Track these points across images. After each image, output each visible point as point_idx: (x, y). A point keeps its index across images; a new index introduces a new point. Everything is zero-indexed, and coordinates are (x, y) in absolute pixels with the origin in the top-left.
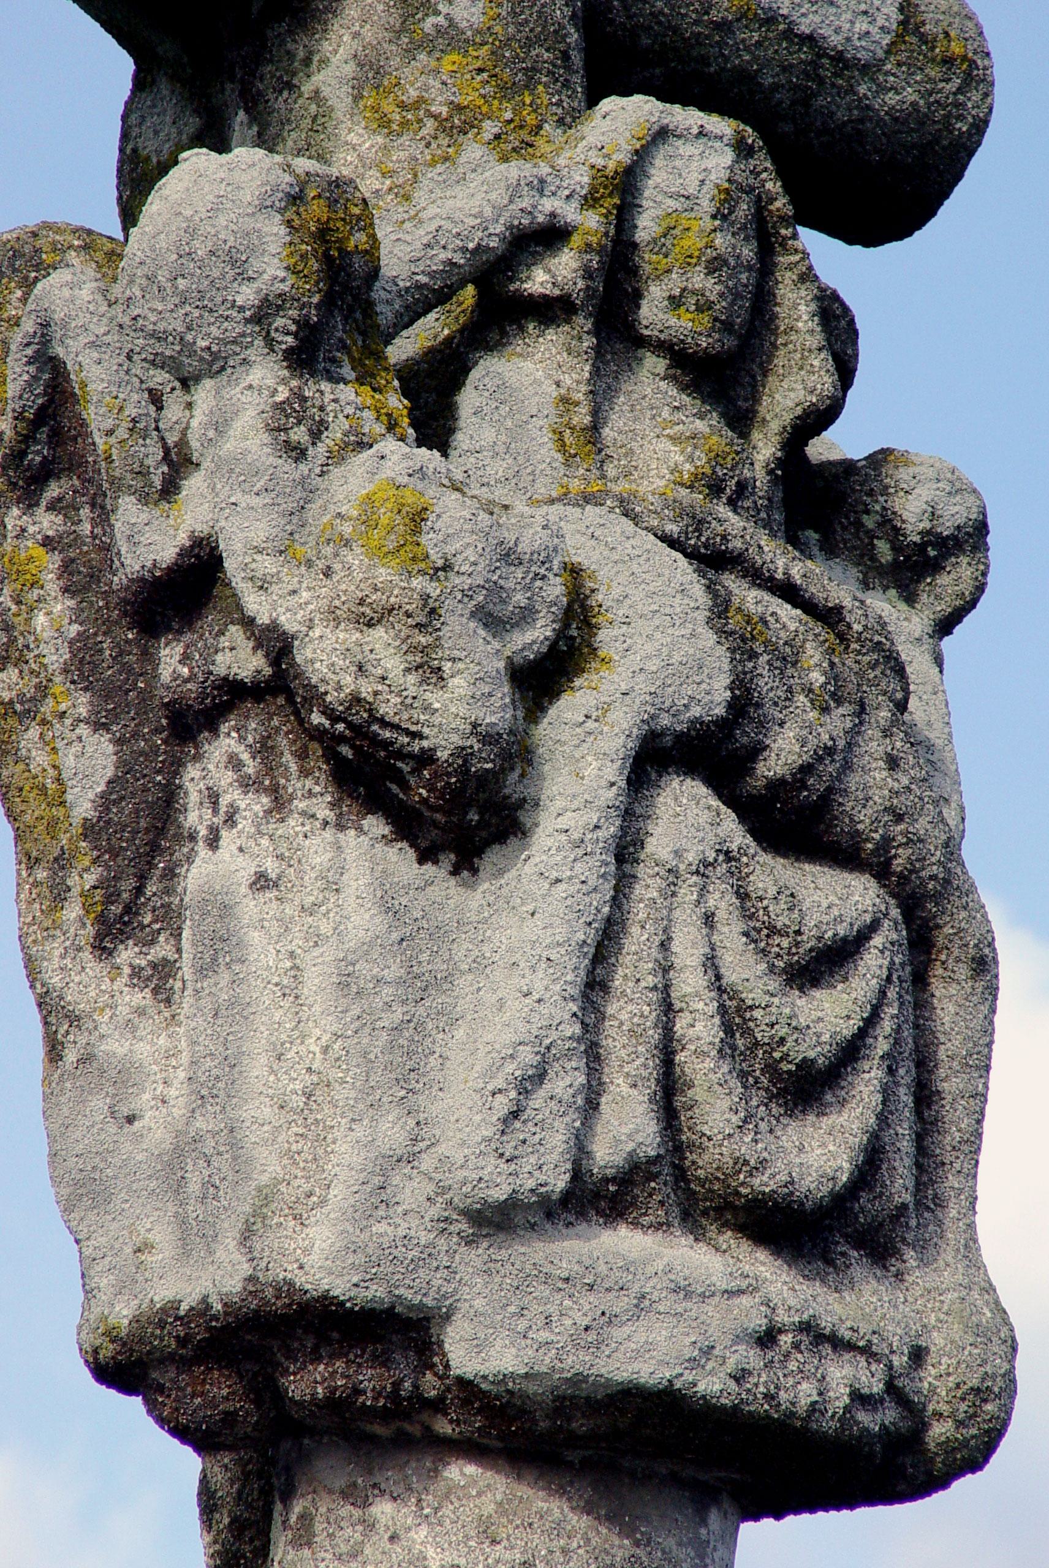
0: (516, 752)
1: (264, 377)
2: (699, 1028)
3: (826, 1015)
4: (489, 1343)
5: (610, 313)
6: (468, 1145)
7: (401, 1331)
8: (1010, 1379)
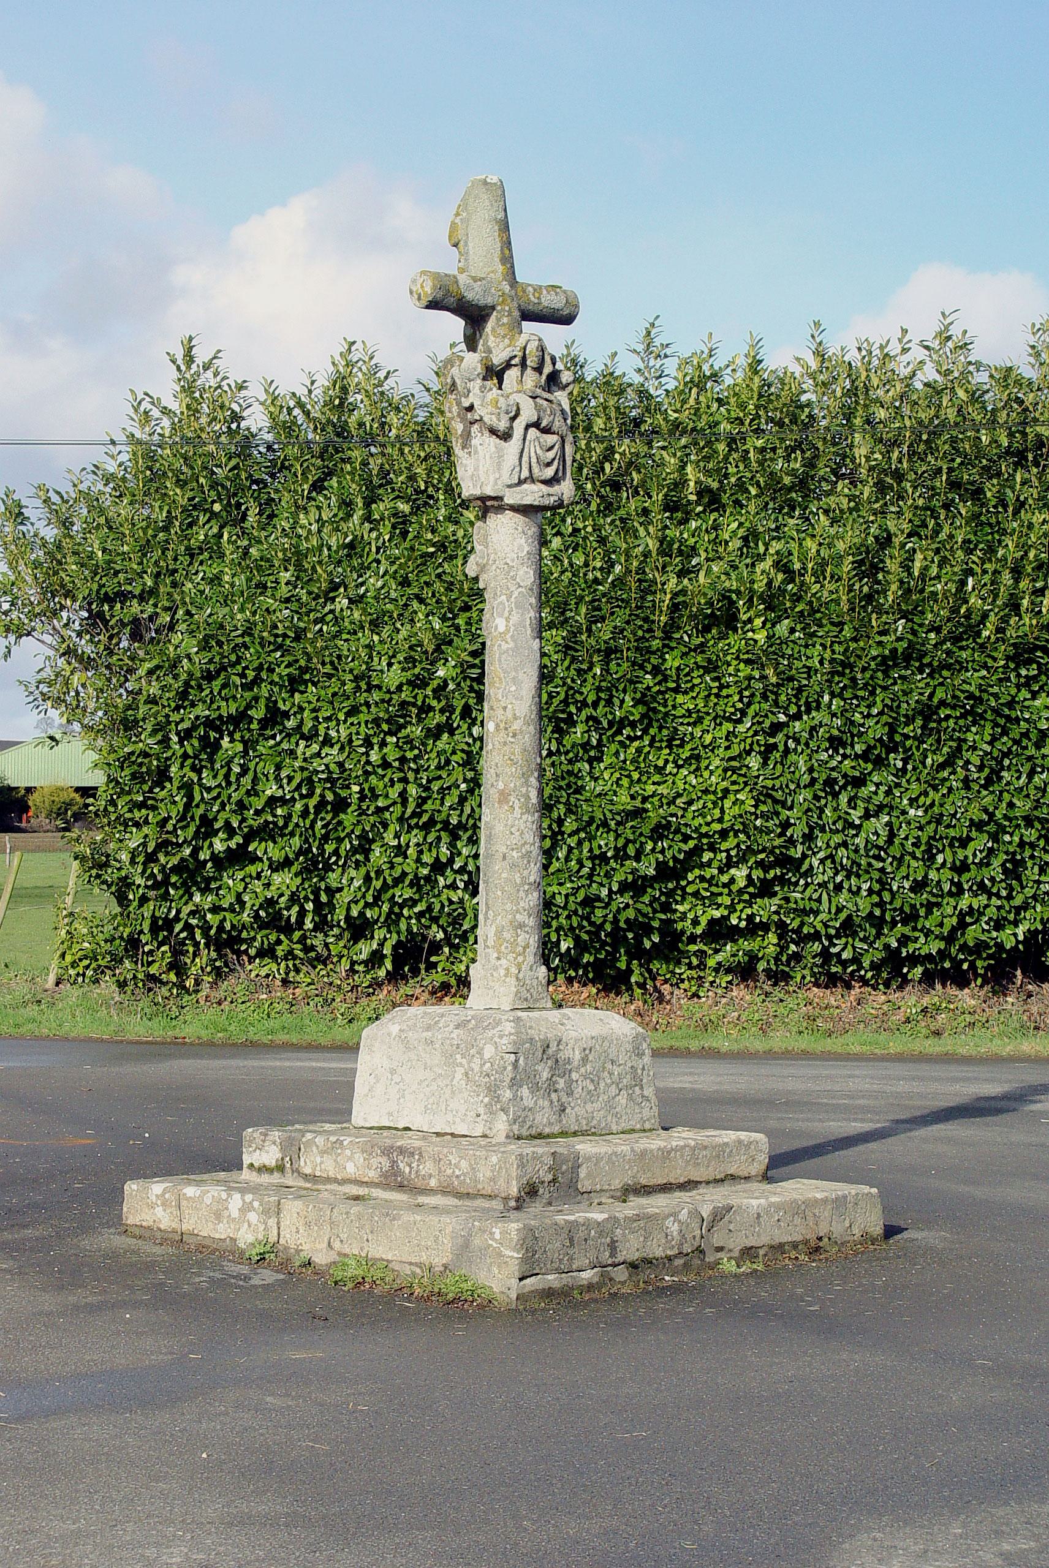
0: (511, 428)
1: (479, 381)
2: (534, 460)
3: (551, 455)
4: (508, 500)
5: (523, 364)
7: (501, 498)
8: (358, 1044)
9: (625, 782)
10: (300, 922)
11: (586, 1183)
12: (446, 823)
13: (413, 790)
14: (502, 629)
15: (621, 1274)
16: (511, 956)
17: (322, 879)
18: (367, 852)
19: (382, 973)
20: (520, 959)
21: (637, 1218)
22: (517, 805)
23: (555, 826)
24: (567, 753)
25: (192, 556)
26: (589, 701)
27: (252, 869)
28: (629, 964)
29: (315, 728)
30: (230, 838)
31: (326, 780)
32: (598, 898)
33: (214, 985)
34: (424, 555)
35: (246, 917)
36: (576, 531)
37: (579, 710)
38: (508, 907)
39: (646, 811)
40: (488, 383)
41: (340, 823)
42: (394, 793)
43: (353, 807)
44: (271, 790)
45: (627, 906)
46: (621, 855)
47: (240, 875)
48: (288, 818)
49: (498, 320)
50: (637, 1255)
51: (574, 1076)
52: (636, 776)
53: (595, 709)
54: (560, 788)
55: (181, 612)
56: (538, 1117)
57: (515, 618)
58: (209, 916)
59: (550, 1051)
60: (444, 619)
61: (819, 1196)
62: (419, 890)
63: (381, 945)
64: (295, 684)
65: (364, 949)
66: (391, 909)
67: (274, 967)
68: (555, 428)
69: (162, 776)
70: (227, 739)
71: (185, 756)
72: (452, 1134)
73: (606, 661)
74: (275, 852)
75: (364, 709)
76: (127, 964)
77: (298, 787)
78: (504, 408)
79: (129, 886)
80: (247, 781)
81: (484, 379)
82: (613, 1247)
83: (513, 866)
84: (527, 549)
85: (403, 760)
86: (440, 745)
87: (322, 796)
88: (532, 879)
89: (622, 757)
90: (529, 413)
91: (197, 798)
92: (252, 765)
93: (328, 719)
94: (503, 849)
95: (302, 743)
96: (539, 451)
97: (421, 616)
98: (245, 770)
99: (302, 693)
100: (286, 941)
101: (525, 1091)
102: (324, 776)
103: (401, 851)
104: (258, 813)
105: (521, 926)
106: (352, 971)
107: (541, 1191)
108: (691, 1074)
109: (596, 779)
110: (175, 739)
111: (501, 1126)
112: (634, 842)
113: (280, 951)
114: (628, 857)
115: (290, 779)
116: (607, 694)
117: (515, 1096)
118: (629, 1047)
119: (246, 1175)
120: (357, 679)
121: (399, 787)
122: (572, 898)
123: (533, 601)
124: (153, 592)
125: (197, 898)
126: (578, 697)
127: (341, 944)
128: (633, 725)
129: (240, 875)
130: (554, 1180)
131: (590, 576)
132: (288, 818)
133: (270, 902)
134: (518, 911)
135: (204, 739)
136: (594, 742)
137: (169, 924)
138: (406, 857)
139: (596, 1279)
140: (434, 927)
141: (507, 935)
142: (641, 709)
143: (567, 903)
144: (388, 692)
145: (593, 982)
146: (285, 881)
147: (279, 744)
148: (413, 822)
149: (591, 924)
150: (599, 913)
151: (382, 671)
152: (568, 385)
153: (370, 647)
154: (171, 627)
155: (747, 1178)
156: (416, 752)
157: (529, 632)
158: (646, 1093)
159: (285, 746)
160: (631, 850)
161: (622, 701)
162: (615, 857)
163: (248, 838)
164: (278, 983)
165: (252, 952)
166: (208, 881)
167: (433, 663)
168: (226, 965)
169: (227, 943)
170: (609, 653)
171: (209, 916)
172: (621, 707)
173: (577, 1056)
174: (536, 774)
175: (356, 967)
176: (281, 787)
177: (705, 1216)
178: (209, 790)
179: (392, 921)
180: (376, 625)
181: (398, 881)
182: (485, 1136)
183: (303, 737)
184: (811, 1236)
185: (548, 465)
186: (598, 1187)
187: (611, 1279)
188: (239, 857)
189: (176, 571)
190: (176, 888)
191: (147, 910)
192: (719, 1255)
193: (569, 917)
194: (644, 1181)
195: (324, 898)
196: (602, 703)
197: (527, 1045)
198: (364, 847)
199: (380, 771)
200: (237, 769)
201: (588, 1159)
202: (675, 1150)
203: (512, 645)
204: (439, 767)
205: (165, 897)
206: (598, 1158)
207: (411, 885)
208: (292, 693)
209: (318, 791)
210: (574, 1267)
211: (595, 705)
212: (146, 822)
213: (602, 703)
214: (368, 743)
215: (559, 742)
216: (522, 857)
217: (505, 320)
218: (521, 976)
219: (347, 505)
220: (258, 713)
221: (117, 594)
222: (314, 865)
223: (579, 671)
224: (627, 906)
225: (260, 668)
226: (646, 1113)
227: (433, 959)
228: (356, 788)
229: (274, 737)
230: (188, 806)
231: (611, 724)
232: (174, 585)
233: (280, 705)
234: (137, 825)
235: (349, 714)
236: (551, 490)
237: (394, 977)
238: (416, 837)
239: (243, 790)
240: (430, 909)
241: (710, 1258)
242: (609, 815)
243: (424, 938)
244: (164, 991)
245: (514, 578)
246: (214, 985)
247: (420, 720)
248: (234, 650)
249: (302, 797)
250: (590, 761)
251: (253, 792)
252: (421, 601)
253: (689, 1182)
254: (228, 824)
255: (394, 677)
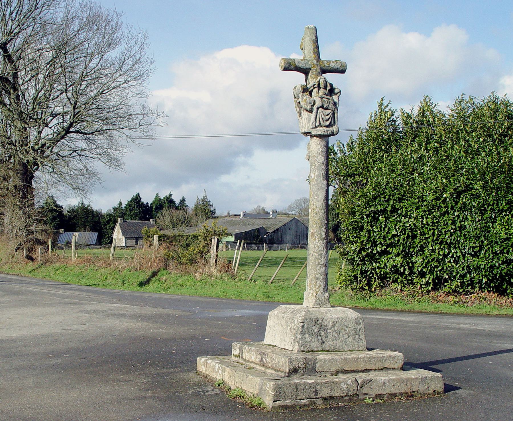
1: (301, 94)
2: (321, 119)
5: (319, 87)
6: (311, 126)
9: (503, 229)
10: (404, 273)
11: (320, 368)
12: (447, 243)
13: (436, 232)
14: (313, 177)
15: (320, 402)
16: (314, 289)
17: (410, 259)
18: (423, 251)
19: (430, 288)
20: (317, 290)
21: (328, 382)
22: (317, 237)
23: (480, 243)
24: (485, 220)
25: (374, 162)
26: (491, 203)
27: (390, 256)
28: (507, 287)
29: (407, 213)
30: (382, 247)
31: (410, 229)
32: (495, 266)
33: (380, 290)
34: (443, 159)
35: (388, 270)
36: (490, 151)
37: (488, 207)
38: (313, 272)
39: (510, 238)
40: (305, 94)
41: (414, 242)
42: (430, 233)
43: (419, 237)
44: (394, 232)
45: (505, 268)
46: (502, 252)
47: (386, 258)
48: (398, 241)
49: (312, 73)
50: (327, 395)
51: (329, 331)
52: (507, 227)
53: (493, 206)
54: (483, 231)
55: (369, 179)
56: (312, 345)
57: (317, 174)
58: (377, 270)
59: (318, 322)
60: (446, 179)
61: (413, 377)
62: (439, 263)
63: (429, 279)
64: (400, 200)
65: (424, 281)
66: (431, 268)
67: (397, 285)
68: (329, 108)
69: (362, 228)
70: (381, 217)
71: (368, 222)
72: (285, 349)
73: (497, 191)
74: (395, 251)
75: (421, 207)
76: (355, 284)
77: (401, 232)
78: (309, 102)
79: (354, 261)
80: (386, 229)
81: (303, 92)
82: (316, 392)
83: (315, 258)
84: (321, 150)
85: (433, 223)
86: (445, 218)
87: (408, 234)
88: (322, 263)
89: (503, 221)
90: (318, 103)
91: (372, 234)
92: (388, 225)
93: (410, 211)
94: (312, 253)
95: (403, 218)
96: (323, 116)
97: (439, 178)
98: (386, 226)
99: (403, 203)
100: (401, 278)
101: (307, 336)
102: (409, 228)
103: (433, 251)
104: (390, 239)
105: (318, 279)
106: (421, 287)
107: (299, 371)
108: (492, 324)
109: (494, 229)
110: (365, 217)
111: (296, 348)
112: (506, 248)
113: (399, 281)
114: (505, 253)
115: (399, 229)
116: (497, 200)
117: (302, 338)
118: (354, 321)
119: (233, 357)
120: (418, 198)
121: (432, 231)
122: (486, 266)
123: (324, 167)
124: (361, 173)
125: (374, 264)
126: (487, 203)
127: (417, 279)
128: (505, 211)
129: (386, 258)
130: (306, 367)
131: (493, 165)
132: (398, 241)
133: (395, 266)
134: (317, 274)
135: (374, 217)
136: (493, 217)
137: (366, 272)
138: (435, 253)
139: (307, 403)
140: (445, 274)
141: (313, 282)
142: (508, 206)
143: (485, 267)
144: (428, 202)
145: (496, 292)
146: (399, 259)
147: (396, 218)
148: (436, 242)
149: (493, 274)
150: (496, 271)
151: (427, 196)
152: (338, 93)
153: (423, 188)
154: (366, 183)
155: (393, 369)
156: (437, 220)
157: (322, 178)
158: (360, 337)
159: (398, 219)
160: (505, 251)
161: (502, 204)
162: (500, 253)
163: (387, 246)
164: (399, 290)
165: (391, 281)
166: (377, 259)
167: (442, 193)
168: (384, 284)
169: (383, 278)
170: (498, 189)
171: (377, 270)
172: (501, 205)
173: (331, 324)
174: (325, 227)
175: (423, 286)
176: (397, 231)
177: (359, 382)
178: (375, 232)
179: (431, 272)
180: (425, 182)
181: (433, 260)
182: (292, 350)
183: (403, 216)
184: (409, 391)
185: (327, 120)
186: (325, 370)
187: (315, 403)
188: (385, 253)
189: (369, 167)
190: (367, 262)
191: (359, 268)
192: (365, 396)
193: (485, 272)
194: (345, 369)
195: (411, 265)
196: (495, 204)
197: (308, 320)
198: (422, 249)
199: (426, 226)
200: (383, 226)
201: (321, 360)
202: (361, 358)
203: (316, 182)
204: (444, 225)
205: (364, 264)
206: (325, 361)
207: (437, 261)
208: (400, 202)
209: (407, 233)
210: (298, 398)
211: (493, 205)
212: (357, 242)
213: (495, 204)
214: (422, 217)
215: (482, 217)
216: (319, 255)
217: (314, 73)
218: (317, 296)
219: (420, 145)
220: (389, 209)
221: (352, 175)
222: (407, 255)
223: (488, 195)
224: (505, 268)
225: (390, 196)
226: (360, 344)
227: (445, 284)
228: (419, 232)
229: (394, 216)
230: (369, 237)
231: (499, 211)
232: (368, 171)
233: (396, 206)
234: (355, 243)
235: (417, 209)
236: (328, 129)
237: (435, 289)
238: (438, 246)
239: (385, 233)
240: (443, 268)
241: (361, 397)
242: (498, 240)
243: (442, 277)
244: (366, 292)
245: (316, 160)
246: (380, 290)
247: (438, 210)
248: (383, 190)
249: (403, 234)
250: (492, 223)
251: (388, 233)
252: (440, 174)
253: (367, 369)
254: (381, 242)
255: (430, 198)
